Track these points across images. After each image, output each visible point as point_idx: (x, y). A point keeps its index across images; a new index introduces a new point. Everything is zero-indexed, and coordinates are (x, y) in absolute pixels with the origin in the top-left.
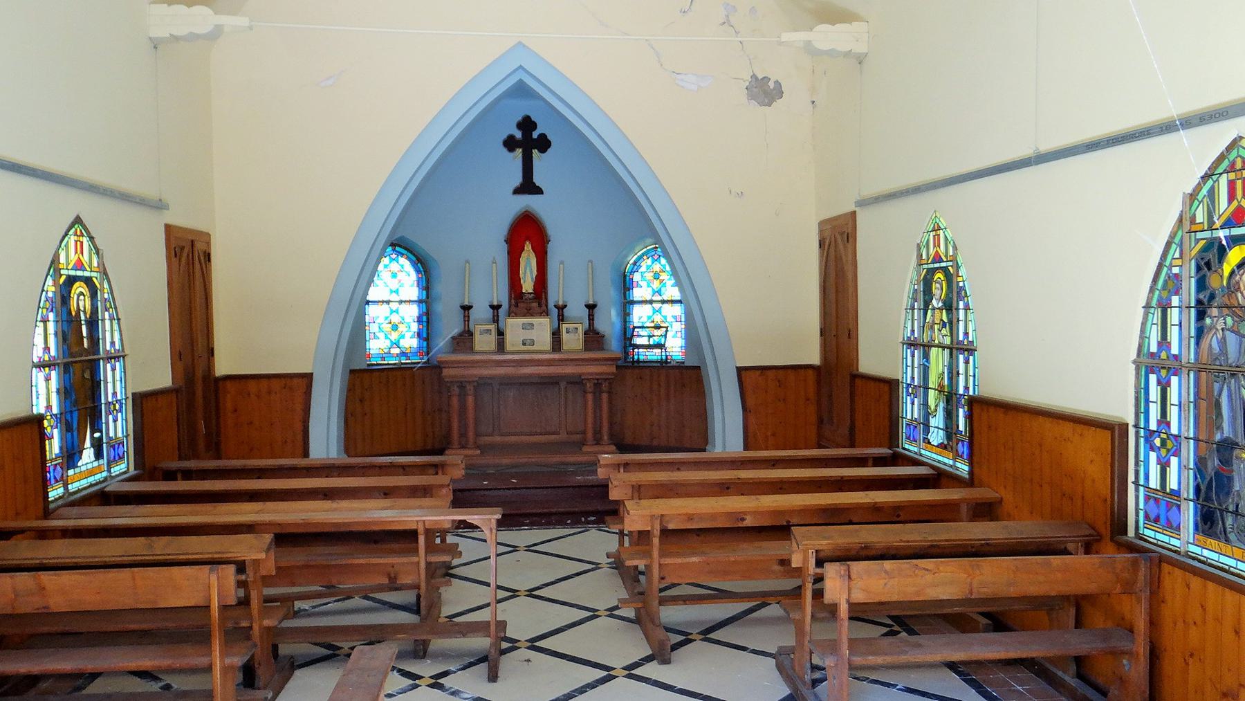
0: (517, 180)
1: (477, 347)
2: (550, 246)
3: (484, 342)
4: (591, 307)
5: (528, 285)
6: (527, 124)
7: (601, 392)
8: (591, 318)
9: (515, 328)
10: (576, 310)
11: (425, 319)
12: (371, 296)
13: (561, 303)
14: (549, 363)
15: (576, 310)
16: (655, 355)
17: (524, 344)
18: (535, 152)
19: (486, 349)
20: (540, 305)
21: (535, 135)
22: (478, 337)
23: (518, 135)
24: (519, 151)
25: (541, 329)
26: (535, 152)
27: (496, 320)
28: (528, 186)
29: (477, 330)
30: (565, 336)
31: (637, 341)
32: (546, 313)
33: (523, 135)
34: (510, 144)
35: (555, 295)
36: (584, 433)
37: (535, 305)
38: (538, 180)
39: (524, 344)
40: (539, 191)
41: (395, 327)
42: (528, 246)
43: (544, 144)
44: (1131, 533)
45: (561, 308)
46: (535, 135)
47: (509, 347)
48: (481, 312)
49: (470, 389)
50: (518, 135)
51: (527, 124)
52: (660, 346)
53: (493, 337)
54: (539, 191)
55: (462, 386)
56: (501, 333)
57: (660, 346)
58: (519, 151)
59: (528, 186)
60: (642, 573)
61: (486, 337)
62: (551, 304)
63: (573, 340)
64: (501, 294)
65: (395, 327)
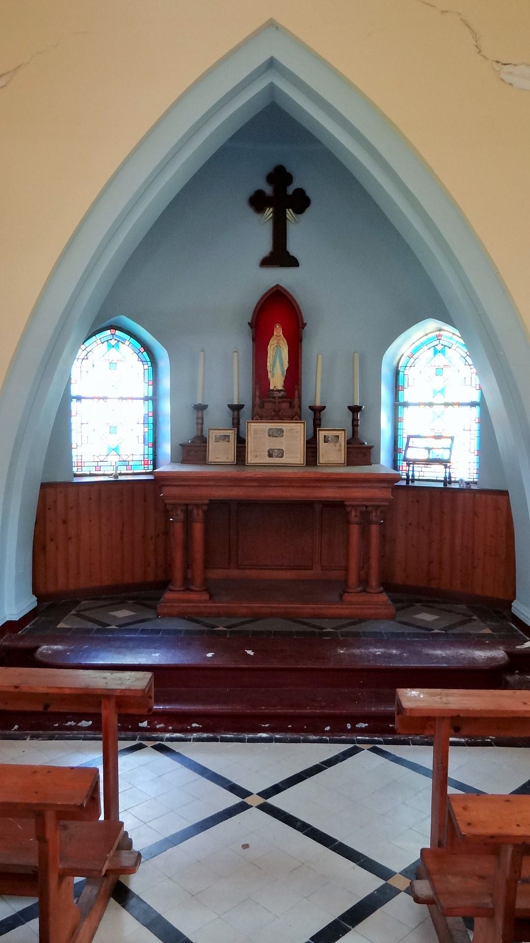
0: (265, 247)
1: (212, 458)
2: (25, 689)
3: (221, 452)
4: (355, 410)
5: (277, 381)
6: (280, 177)
7: (370, 523)
8: (355, 424)
9: (258, 434)
10: (337, 417)
11: (151, 420)
12: (74, 392)
13: (318, 404)
14: (304, 482)
15: (337, 417)
16: (434, 474)
17: (270, 455)
18: (289, 213)
19: (222, 459)
20: (291, 406)
21: (290, 190)
22: (212, 445)
23: (268, 190)
24: (269, 212)
25: (294, 434)
26: (289, 213)
27: (236, 423)
28: (280, 256)
29: (212, 436)
30: (322, 446)
31: (411, 454)
32: (295, 416)
33: (270, 206)
34: (258, 202)
35: (314, 390)
36: (346, 569)
37: (285, 405)
38: (293, 247)
39: (270, 455)
40: (293, 262)
41: (113, 430)
42: (278, 331)
43: (301, 202)
44: (385, 457)
45: (317, 411)
46: (290, 190)
47: (251, 459)
48: (218, 417)
49: (198, 514)
50: (268, 190)
51: (280, 177)
52: (445, 463)
53: (232, 445)
54: (293, 262)
55: (188, 511)
56: (241, 442)
57: (445, 463)
58: (269, 212)
59: (280, 256)
60: (341, 596)
61: (222, 444)
62: (306, 402)
63: (332, 454)
64: (239, 388)
65: (113, 430)
